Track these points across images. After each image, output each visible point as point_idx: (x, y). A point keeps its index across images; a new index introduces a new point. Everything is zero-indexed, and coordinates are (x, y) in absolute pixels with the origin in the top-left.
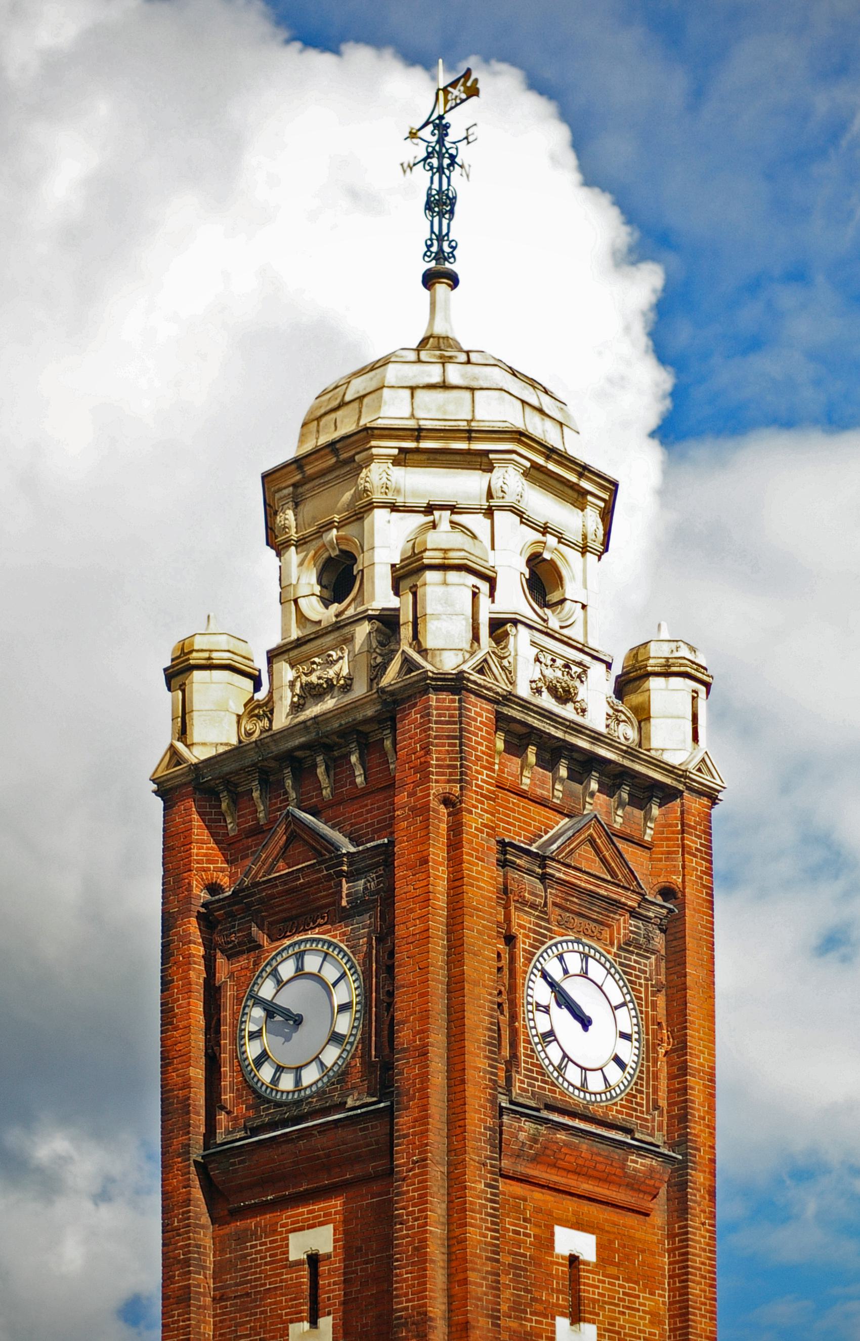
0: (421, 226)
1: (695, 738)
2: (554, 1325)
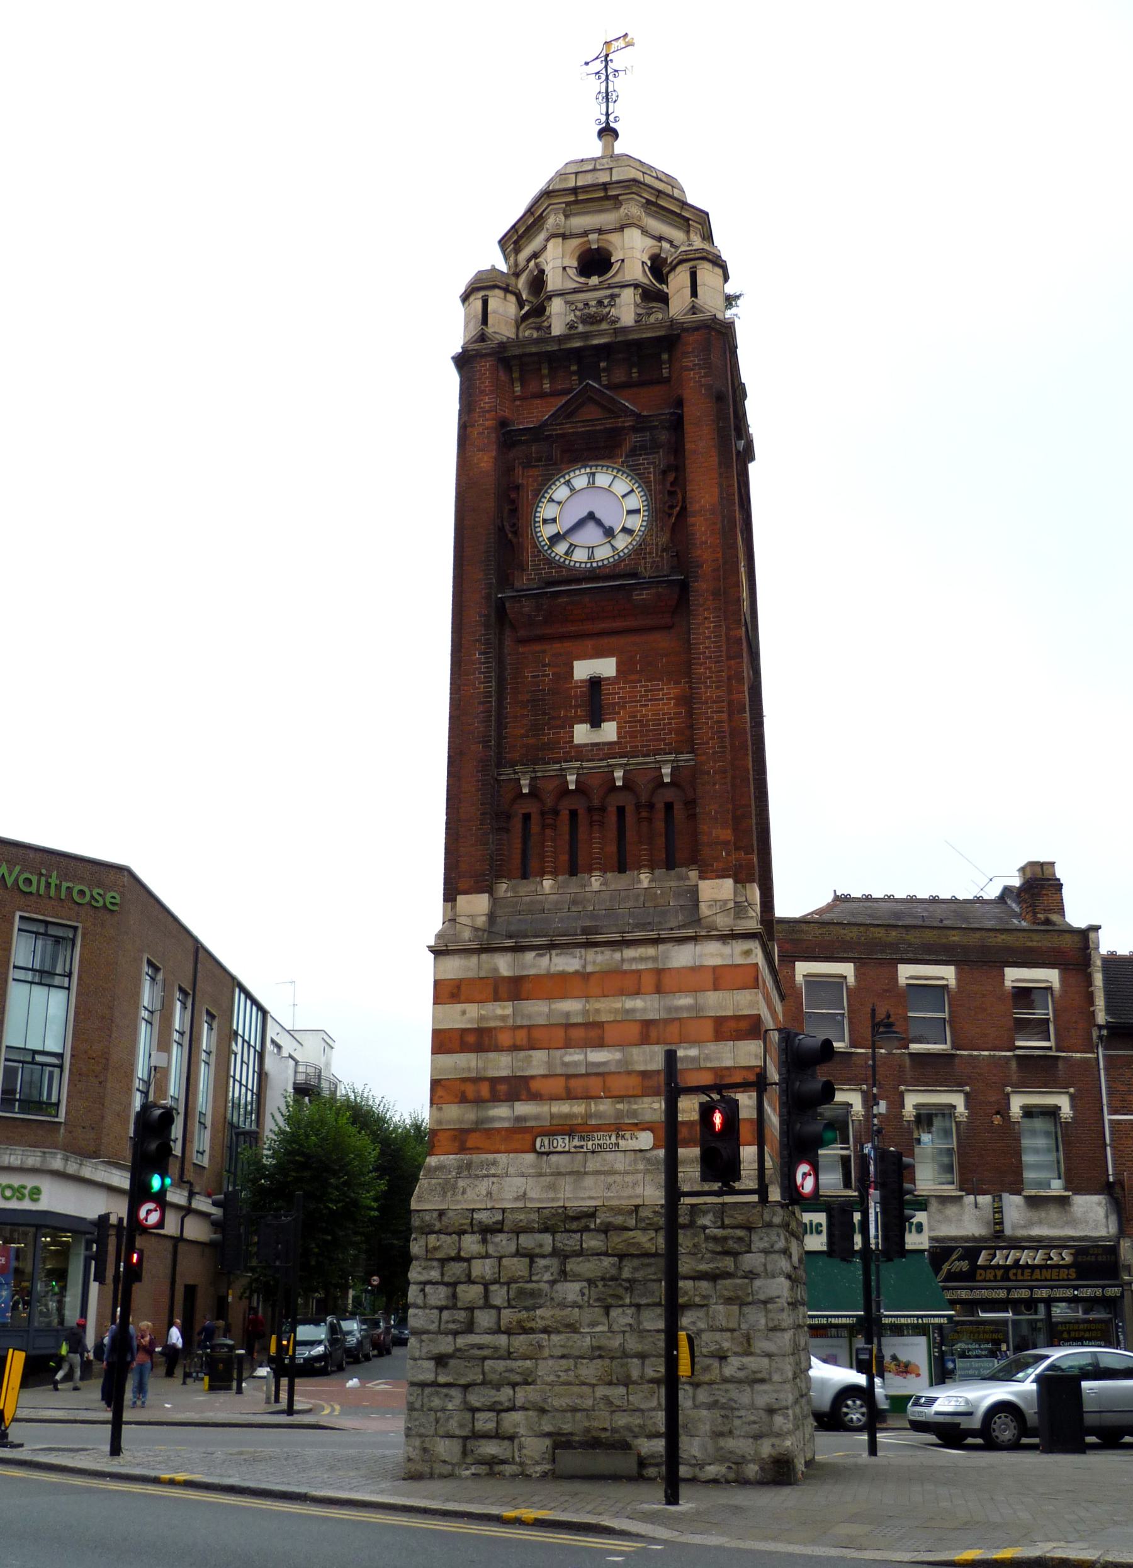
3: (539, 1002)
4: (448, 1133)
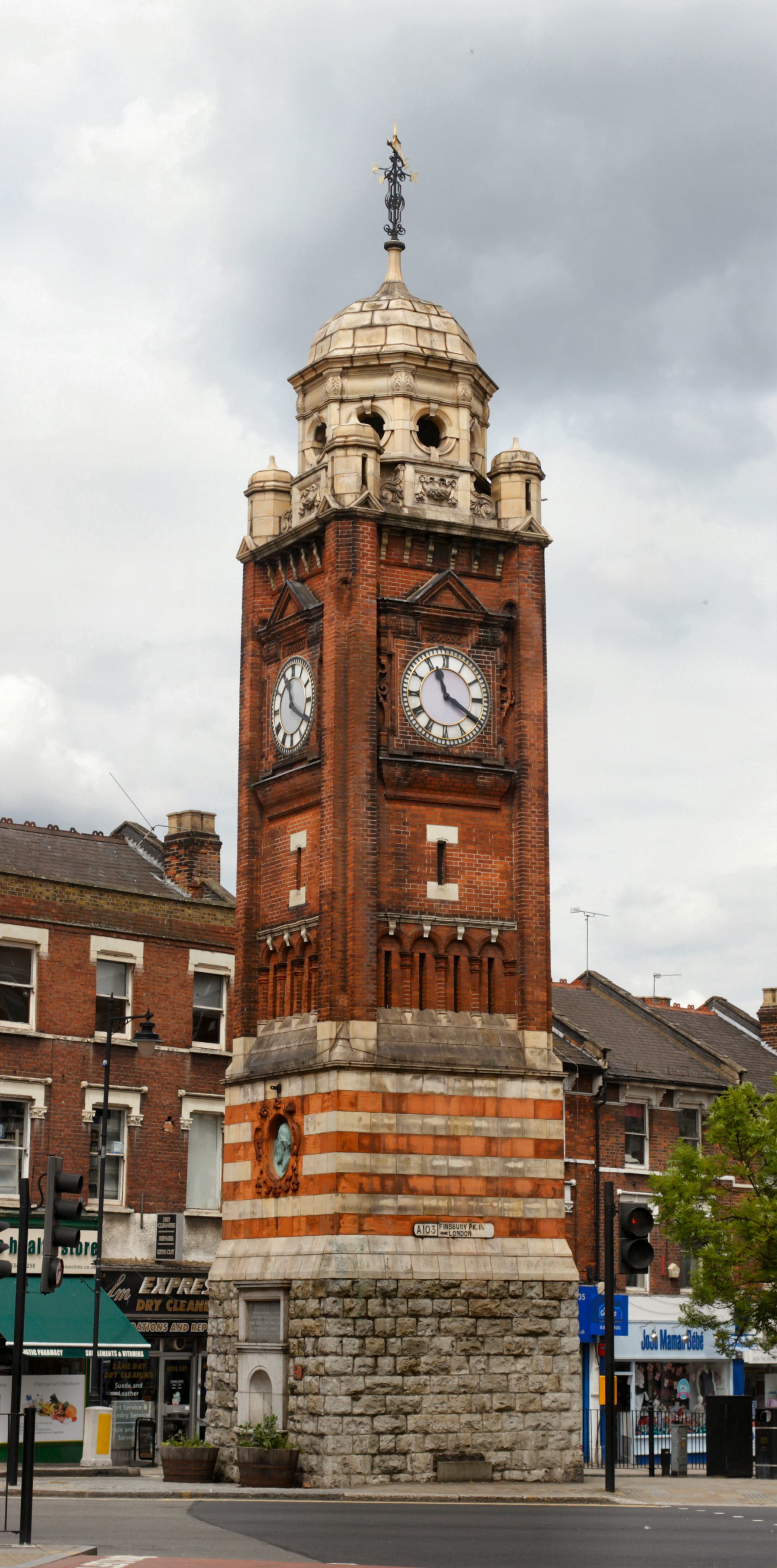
0: (383, 216)
1: (528, 506)
2: (426, 887)
3: (415, 1116)
4: (350, 1217)
